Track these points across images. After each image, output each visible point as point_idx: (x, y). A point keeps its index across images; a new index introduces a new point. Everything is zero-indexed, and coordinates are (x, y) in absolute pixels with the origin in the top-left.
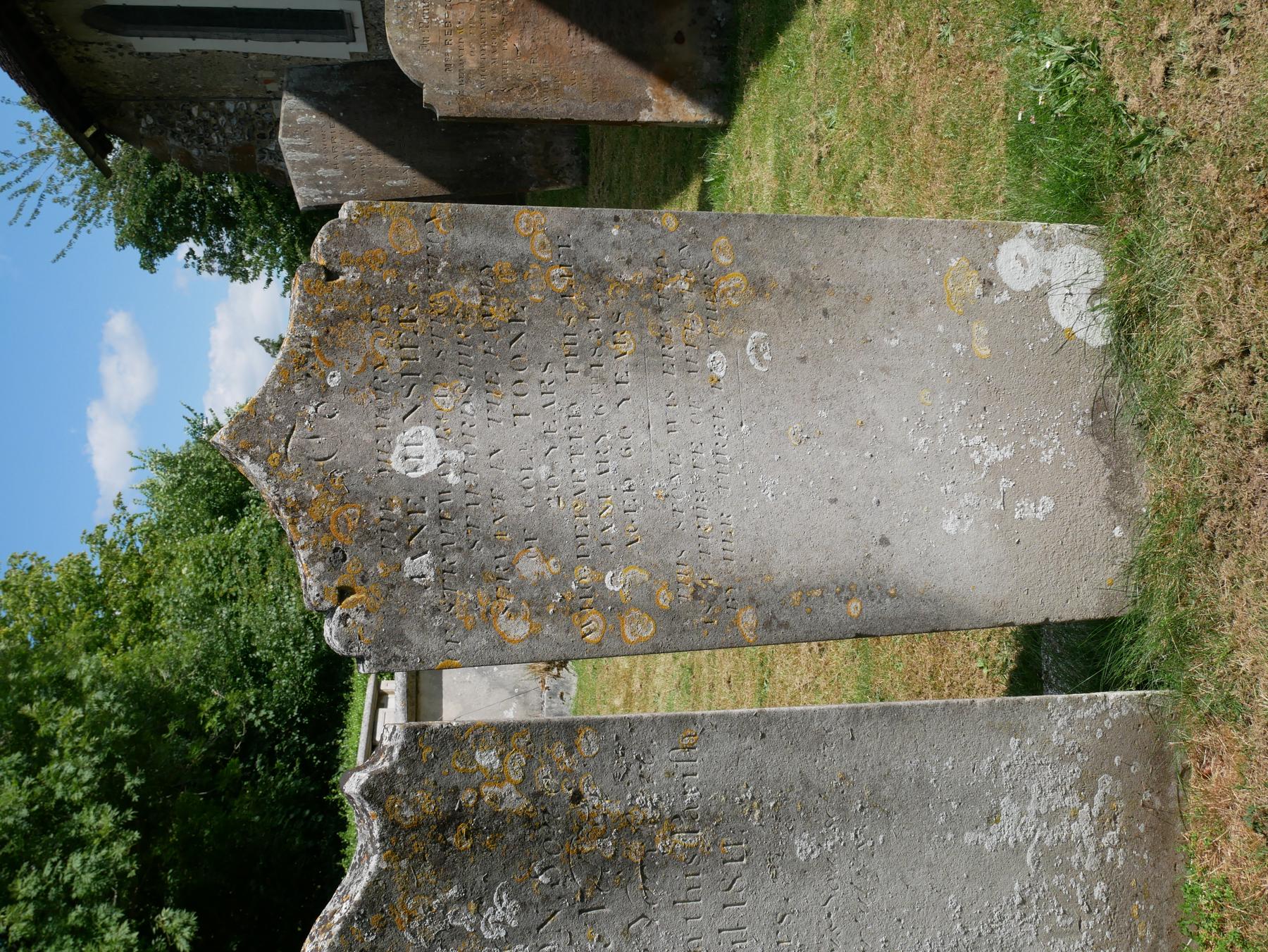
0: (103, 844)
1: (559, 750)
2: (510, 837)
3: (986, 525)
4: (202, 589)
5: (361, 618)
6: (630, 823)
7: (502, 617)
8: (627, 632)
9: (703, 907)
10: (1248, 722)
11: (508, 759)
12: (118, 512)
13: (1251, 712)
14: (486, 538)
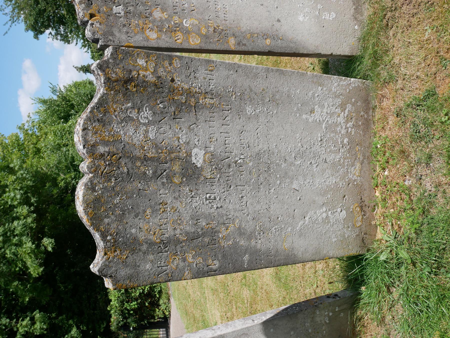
0: (25, 218)
1: (166, 63)
2: (149, 90)
3: (313, 19)
4: (57, 142)
5: (98, 25)
6: (191, 92)
7: (148, 31)
8: (191, 41)
9: (216, 124)
10: (397, 81)
11: (149, 63)
12: (29, 119)
13: (398, 77)
14: (142, 3)
